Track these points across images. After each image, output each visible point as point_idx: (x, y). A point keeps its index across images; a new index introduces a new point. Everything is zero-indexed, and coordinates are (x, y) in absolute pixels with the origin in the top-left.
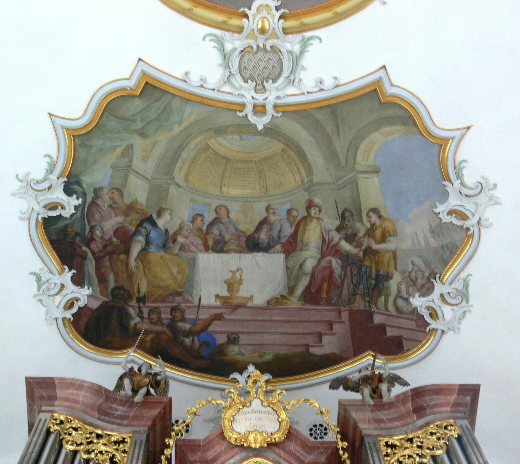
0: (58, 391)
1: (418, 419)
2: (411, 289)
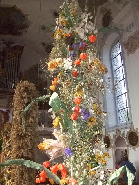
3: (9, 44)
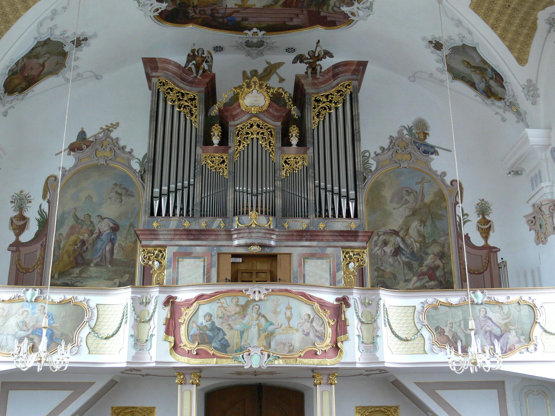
0: (159, 64)
1: (334, 81)
2: (341, 4)
3: (312, 60)
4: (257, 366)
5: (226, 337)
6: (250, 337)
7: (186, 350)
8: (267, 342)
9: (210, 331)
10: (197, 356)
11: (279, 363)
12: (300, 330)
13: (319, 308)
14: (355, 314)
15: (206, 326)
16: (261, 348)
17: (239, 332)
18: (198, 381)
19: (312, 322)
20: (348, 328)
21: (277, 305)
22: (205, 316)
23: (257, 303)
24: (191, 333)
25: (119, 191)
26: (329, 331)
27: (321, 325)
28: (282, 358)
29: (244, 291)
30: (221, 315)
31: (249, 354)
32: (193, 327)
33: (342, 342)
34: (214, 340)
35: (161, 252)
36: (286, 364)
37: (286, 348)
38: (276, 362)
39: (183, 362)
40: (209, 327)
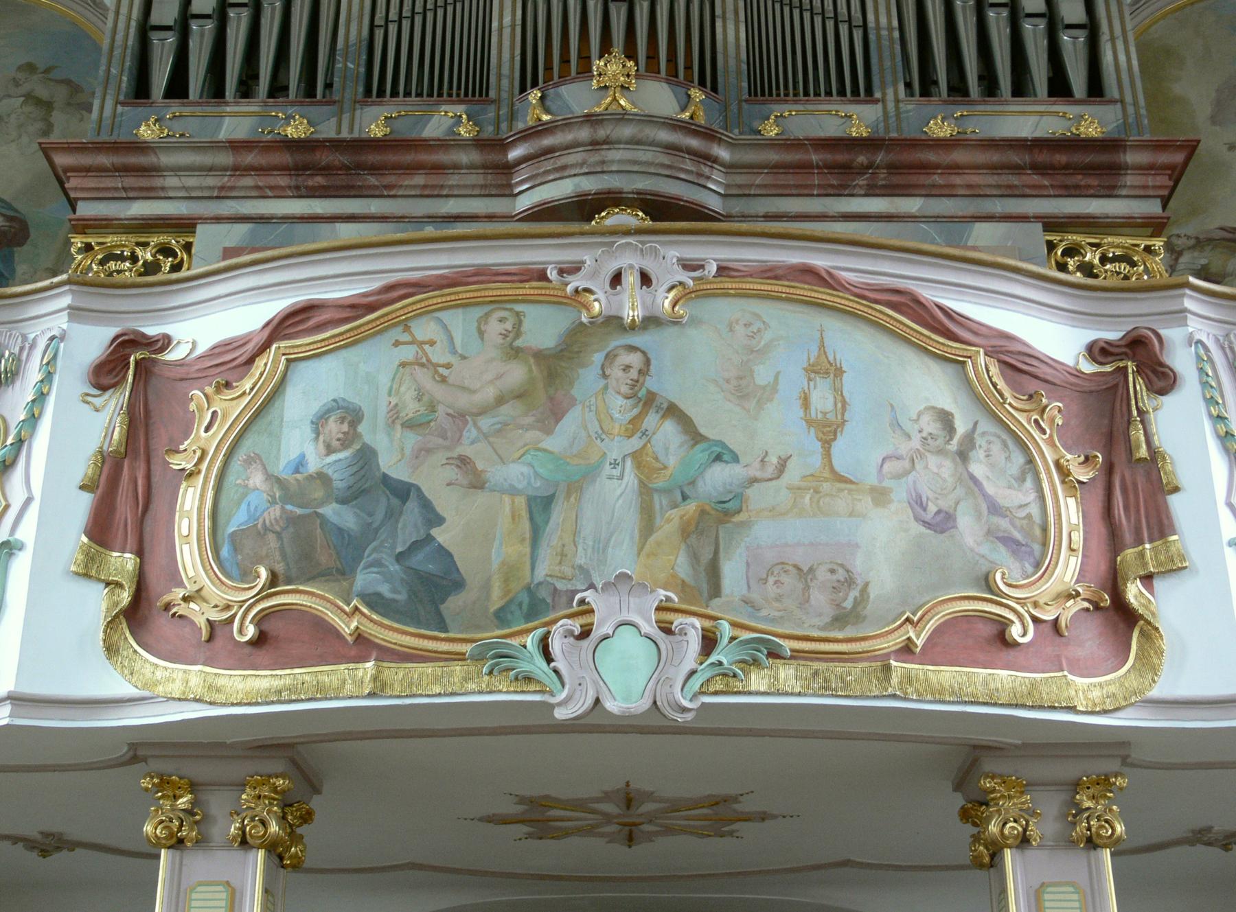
4: (640, 705)
5: (442, 536)
6: (587, 527)
7: (201, 622)
8: (694, 557)
9: (343, 501)
10: (262, 655)
11: (776, 686)
12: (900, 493)
13: (1001, 385)
14: (1207, 426)
15: (322, 477)
16: (662, 593)
17: (521, 501)
18: (274, 828)
19: (963, 455)
20: (1174, 501)
21: (756, 353)
22: (319, 423)
23: (637, 340)
24: (236, 521)
25: (42, 92)
26: (1071, 511)
27: (1021, 479)
28: (796, 655)
29: (552, 274)
30: (411, 408)
31: (585, 634)
32: (246, 490)
33: (1148, 579)
34: (369, 555)
35: (167, 251)
36: (824, 690)
37: (819, 599)
38: (758, 680)
39: (174, 692)
40: (340, 480)
